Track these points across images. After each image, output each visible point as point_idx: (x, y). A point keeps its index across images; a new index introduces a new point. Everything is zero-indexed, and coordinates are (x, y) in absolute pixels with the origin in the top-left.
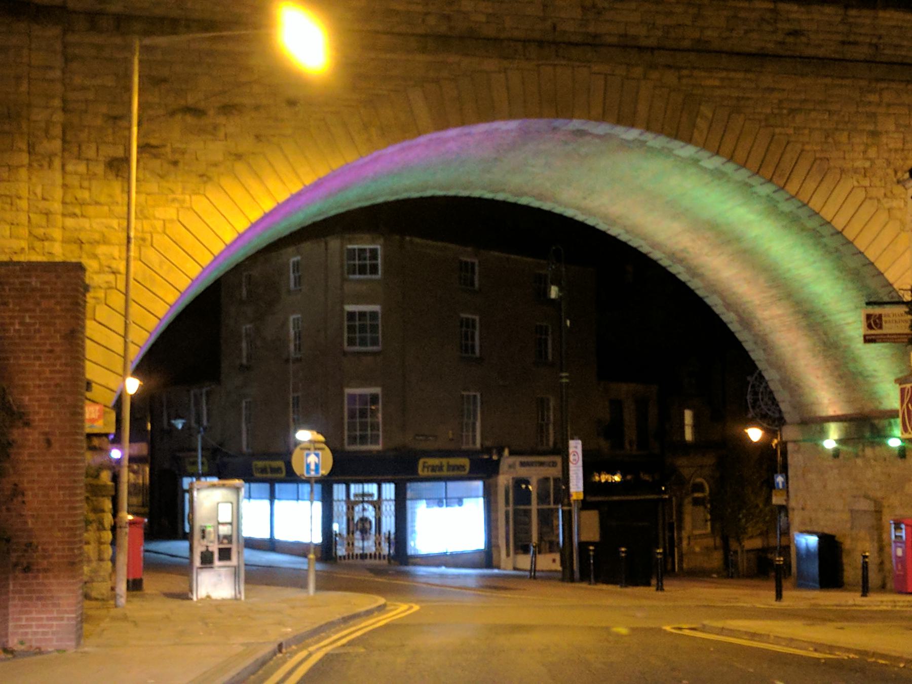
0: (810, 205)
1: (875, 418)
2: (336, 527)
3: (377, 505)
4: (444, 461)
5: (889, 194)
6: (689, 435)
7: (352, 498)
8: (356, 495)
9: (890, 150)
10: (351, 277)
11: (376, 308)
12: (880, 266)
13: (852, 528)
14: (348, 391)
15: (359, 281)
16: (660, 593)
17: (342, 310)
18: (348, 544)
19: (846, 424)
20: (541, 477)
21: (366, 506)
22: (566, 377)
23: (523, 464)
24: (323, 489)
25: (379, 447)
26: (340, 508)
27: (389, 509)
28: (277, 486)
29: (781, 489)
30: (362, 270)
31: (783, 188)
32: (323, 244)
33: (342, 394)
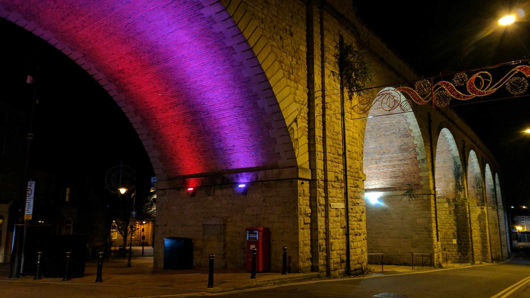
0: (239, 25)
5: (272, 37)
6: (67, 199)
9: (273, 15)
12: (268, 75)
13: (204, 235)
16: (101, 283)
22: (31, 136)
28: (326, 266)
31: (225, 9)
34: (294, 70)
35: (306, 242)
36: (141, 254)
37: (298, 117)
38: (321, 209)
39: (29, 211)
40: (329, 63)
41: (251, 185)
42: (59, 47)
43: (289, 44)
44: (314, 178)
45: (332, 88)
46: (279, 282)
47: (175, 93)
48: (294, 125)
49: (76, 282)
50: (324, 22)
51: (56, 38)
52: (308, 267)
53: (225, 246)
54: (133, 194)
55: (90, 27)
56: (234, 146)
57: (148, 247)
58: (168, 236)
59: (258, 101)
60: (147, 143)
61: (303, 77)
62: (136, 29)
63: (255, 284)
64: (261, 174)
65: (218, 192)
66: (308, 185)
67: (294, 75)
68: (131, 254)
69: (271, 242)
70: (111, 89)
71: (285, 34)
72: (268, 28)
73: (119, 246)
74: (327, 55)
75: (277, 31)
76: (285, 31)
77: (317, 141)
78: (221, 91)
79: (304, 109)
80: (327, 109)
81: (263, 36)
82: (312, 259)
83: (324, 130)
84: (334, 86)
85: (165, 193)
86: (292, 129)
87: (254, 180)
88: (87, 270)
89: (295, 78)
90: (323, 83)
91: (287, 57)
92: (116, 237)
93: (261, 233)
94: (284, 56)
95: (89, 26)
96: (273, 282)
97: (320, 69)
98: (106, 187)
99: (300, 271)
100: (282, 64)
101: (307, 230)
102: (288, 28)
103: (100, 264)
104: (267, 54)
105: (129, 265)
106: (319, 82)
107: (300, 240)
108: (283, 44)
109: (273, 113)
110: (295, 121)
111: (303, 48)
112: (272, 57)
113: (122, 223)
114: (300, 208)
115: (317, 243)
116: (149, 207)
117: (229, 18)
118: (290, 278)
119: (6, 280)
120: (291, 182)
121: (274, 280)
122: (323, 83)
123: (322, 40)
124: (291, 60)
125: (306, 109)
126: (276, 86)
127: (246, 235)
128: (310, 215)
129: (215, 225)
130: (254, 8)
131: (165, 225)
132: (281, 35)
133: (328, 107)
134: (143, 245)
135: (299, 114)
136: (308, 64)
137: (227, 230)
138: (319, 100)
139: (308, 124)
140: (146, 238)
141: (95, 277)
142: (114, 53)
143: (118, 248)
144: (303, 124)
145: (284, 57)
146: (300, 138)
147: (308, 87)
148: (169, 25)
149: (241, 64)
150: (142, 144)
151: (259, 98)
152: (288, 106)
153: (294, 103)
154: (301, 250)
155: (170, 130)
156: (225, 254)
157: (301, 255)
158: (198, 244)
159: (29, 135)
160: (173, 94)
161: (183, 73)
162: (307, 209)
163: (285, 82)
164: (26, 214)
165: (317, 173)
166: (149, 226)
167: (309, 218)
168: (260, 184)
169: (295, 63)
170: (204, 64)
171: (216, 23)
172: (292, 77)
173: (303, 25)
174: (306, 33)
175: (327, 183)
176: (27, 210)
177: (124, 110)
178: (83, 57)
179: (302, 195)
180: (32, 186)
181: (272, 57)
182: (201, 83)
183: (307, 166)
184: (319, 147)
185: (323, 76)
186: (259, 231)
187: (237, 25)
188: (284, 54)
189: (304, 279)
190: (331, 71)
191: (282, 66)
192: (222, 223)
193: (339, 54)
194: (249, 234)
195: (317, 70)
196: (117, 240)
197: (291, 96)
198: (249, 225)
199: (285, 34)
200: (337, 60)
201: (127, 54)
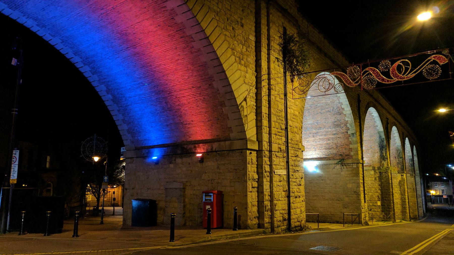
0: (197, 17)
1: (184, 144)
5: (225, 28)
6: (48, 166)
9: (226, 8)
13: (166, 197)
19: (162, 148)
22: (16, 111)
28: (270, 224)
29: (106, 182)
34: (244, 56)
35: (254, 203)
36: (112, 213)
37: (247, 97)
38: (267, 175)
39: (14, 176)
40: (274, 51)
41: (207, 153)
43: (240, 33)
44: (260, 149)
45: (276, 72)
46: (231, 237)
48: (244, 104)
49: (55, 237)
51: (37, 25)
52: (255, 224)
53: (184, 206)
54: (105, 162)
56: (192, 121)
58: (136, 198)
59: (214, 83)
60: (118, 117)
61: (251, 62)
63: (210, 238)
64: (215, 146)
65: (179, 161)
66: (256, 155)
67: (244, 60)
69: (224, 203)
70: (86, 70)
71: (237, 25)
72: (222, 20)
73: (93, 207)
74: (272, 44)
75: (230, 23)
76: (237, 22)
77: (263, 117)
78: (181, 73)
79: (252, 90)
80: (272, 90)
81: (218, 27)
82: (258, 218)
83: (269, 107)
84: (278, 70)
85: (133, 161)
86: (242, 107)
87: (209, 150)
88: (65, 227)
89: (245, 63)
90: (269, 68)
91: (238, 45)
92: (91, 198)
93: (215, 195)
94: (236, 44)
96: (226, 237)
97: (267, 56)
98: (81, 156)
99: (248, 228)
100: (234, 52)
101: (254, 193)
102: (239, 20)
104: (221, 42)
105: (102, 223)
106: (265, 67)
107: (248, 201)
108: (235, 34)
109: (226, 93)
110: (245, 100)
111: (252, 38)
112: (225, 46)
114: (249, 175)
115: (263, 204)
117: (189, 11)
118: (240, 234)
120: (241, 152)
121: (226, 235)
122: (269, 68)
123: (268, 31)
124: (241, 48)
125: (254, 90)
126: (229, 69)
127: (202, 197)
128: (257, 180)
129: (176, 189)
130: (210, 2)
131: (133, 189)
132: (233, 26)
133: (273, 89)
134: (114, 205)
135: (249, 94)
136: (256, 51)
137: (186, 193)
138: (266, 82)
139: (256, 102)
140: (116, 200)
141: (72, 233)
143: (92, 208)
144: (252, 102)
145: (236, 45)
146: (249, 114)
147: (256, 71)
148: (136, 16)
149: (199, 50)
151: (214, 80)
152: (239, 87)
153: (244, 85)
154: (249, 210)
155: (138, 107)
156: (184, 213)
157: (249, 214)
158: (161, 204)
159: (14, 110)
162: (254, 175)
163: (237, 66)
164: (11, 178)
165: (263, 144)
167: (256, 183)
168: (215, 153)
169: (245, 50)
171: (177, 15)
172: (243, 62)
173: (252, 18)
174: (254, 25)
177: (98, 89)
178: (61, 43)
179: (251, 164)
180: (16, 154)
181: (225, 46)
183: (254, 138)
184: (265, 123)
185: (269, 62)
186: (214, 194)
187: (195, 17)
188: (236, 42)
189: (252, 235)
190: (276, 58)
191: (234, 53)
192: (182, 187)
193: (282, 43)
194: (205, 196)
195: (264, 56)
196: (91, 202)
197: (242, 79)
198: (205, 189)
199: (237, 25)
200: (281, 48)
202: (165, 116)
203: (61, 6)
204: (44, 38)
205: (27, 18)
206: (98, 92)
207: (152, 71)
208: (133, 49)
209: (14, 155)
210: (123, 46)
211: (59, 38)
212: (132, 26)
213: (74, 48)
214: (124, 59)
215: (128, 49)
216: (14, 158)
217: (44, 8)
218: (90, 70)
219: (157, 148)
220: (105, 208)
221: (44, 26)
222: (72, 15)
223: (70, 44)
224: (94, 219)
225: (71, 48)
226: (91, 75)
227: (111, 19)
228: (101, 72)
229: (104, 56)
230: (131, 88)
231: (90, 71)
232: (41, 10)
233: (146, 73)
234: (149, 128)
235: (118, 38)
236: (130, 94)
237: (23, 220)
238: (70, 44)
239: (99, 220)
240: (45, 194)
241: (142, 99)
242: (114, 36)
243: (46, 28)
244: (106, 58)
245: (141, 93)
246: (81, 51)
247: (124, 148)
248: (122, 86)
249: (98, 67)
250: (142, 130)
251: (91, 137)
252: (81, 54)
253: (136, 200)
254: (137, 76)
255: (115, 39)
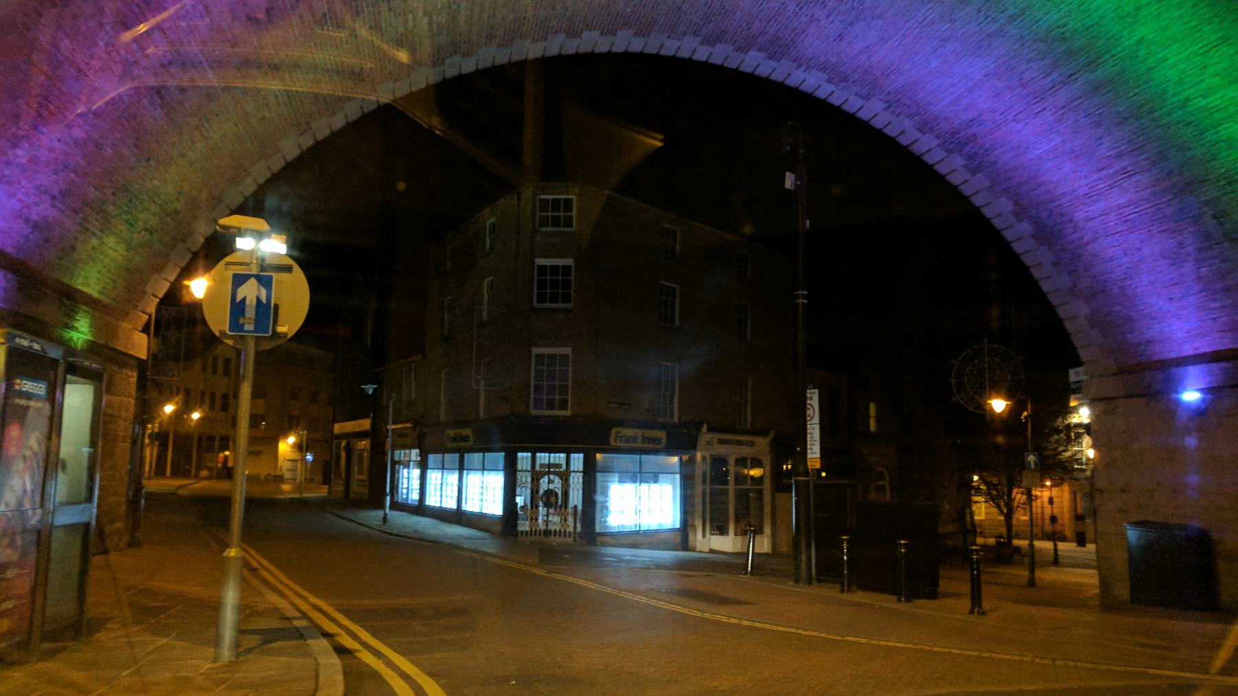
2: (519, 500)
3: (565, 477)
4: (639, 432)
6: (873, 426)
7: (538, 468)
8: (542, 466)
10: (544, 229)
11: (569, 262)
14: (536, 351)
15: (552, 234)
17: (533, 262)
18: (532, 519)
19: (1213, 365)
20: (738, 457)
21: (552, 477)
22: (804, 297)
23: (721, 442)
24: (506, 458)
25: (568, 413)
26: (524, 478)
27: (576, 481)
29: (1032, 470)
30: (556, 222)
32: (515, 198)
33: (530, 352)
36: (1051, 559)
39: (814, 451)
42: (835, 100)
47: (1123, 145)
49: (923, 607)
50: (72, 283)
51: (829, 81)
54: (1025, 414)
55: (897, 37)
57: (1065, 543)
58: (1134, 520)
62: (1006, 9)
68: (1033, 560)
70: (953, 168)
73: (996, 537)
88: (944, 585)
92: (983, 514)
95: (895, 35)
98: (954, 399)
103: (975, 572)
105: (1032, 583)
113: (996, 482)
116: (1062, 445)
119: (790, 586)
131: (1123, 491)
134: (1055, 537)
140: (1060, 522)
141: (966, 603)
142: (955, 82)
143: (992, 541)
150: (1039, 288)
155: (1116, 244)
159: (799, 294)
160: (1117, 150)
161: (1145, 86)
164: (809, 456)
166: (1062, 491)
170: (1210, 47)
175: (552, 464)
176: (811, 449)
180: (813, 399)
182: (1203, 103)
201: (987, 76)
202: (1216, 261)
203: (880, 17)
204: (846, 107)
205: (805, 71)
206: (991, 221)
207: (1158, 127)
208: (1087, 75)
209: (808, 402)
210: (1055, 75)
211: (881, 100)
212: (1083, 7)
213: (918, 114)
214: (1062, 111)
215: (1073, 77)
216: (809, 409)
217: (842, 33)
218: (965, 162)
219: (1196, 364)
220: (1037, 544)
221: (845, 79)
222: (909, 28)
223: (908, 107)
224: (992, 570)
225: (911, 116)
226: (967, 176)
227: (1016, 7)
228: (996, 163)
229: (1000, 117)
230: (1089, 191)
231: (965, 166)
232: (835, 41)
233: (1139, 137)
234: (1161, 303)
235: (1039, 53)
236: (1091, 208)
237: (845, 558)
238: (908, 107)
239: (1023, 576)
240: (873, 496)
241: (1131, 217)
242: (1025, 52)
243: (848, 81)
244: (1006, 120)
245: (1123, 201)
246: (936, 119)
247: (1081, 369)
248: (1060, 192)
249: (986, 150)
250: (1138, 311)
251: (976, 347)
252: (937, 125)
253: (1137, 524)
254: (1109, 151)
255: (1030, 61)
